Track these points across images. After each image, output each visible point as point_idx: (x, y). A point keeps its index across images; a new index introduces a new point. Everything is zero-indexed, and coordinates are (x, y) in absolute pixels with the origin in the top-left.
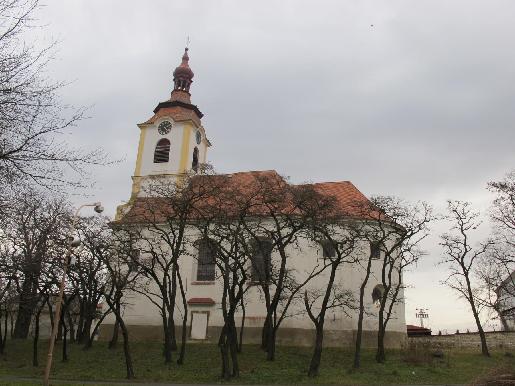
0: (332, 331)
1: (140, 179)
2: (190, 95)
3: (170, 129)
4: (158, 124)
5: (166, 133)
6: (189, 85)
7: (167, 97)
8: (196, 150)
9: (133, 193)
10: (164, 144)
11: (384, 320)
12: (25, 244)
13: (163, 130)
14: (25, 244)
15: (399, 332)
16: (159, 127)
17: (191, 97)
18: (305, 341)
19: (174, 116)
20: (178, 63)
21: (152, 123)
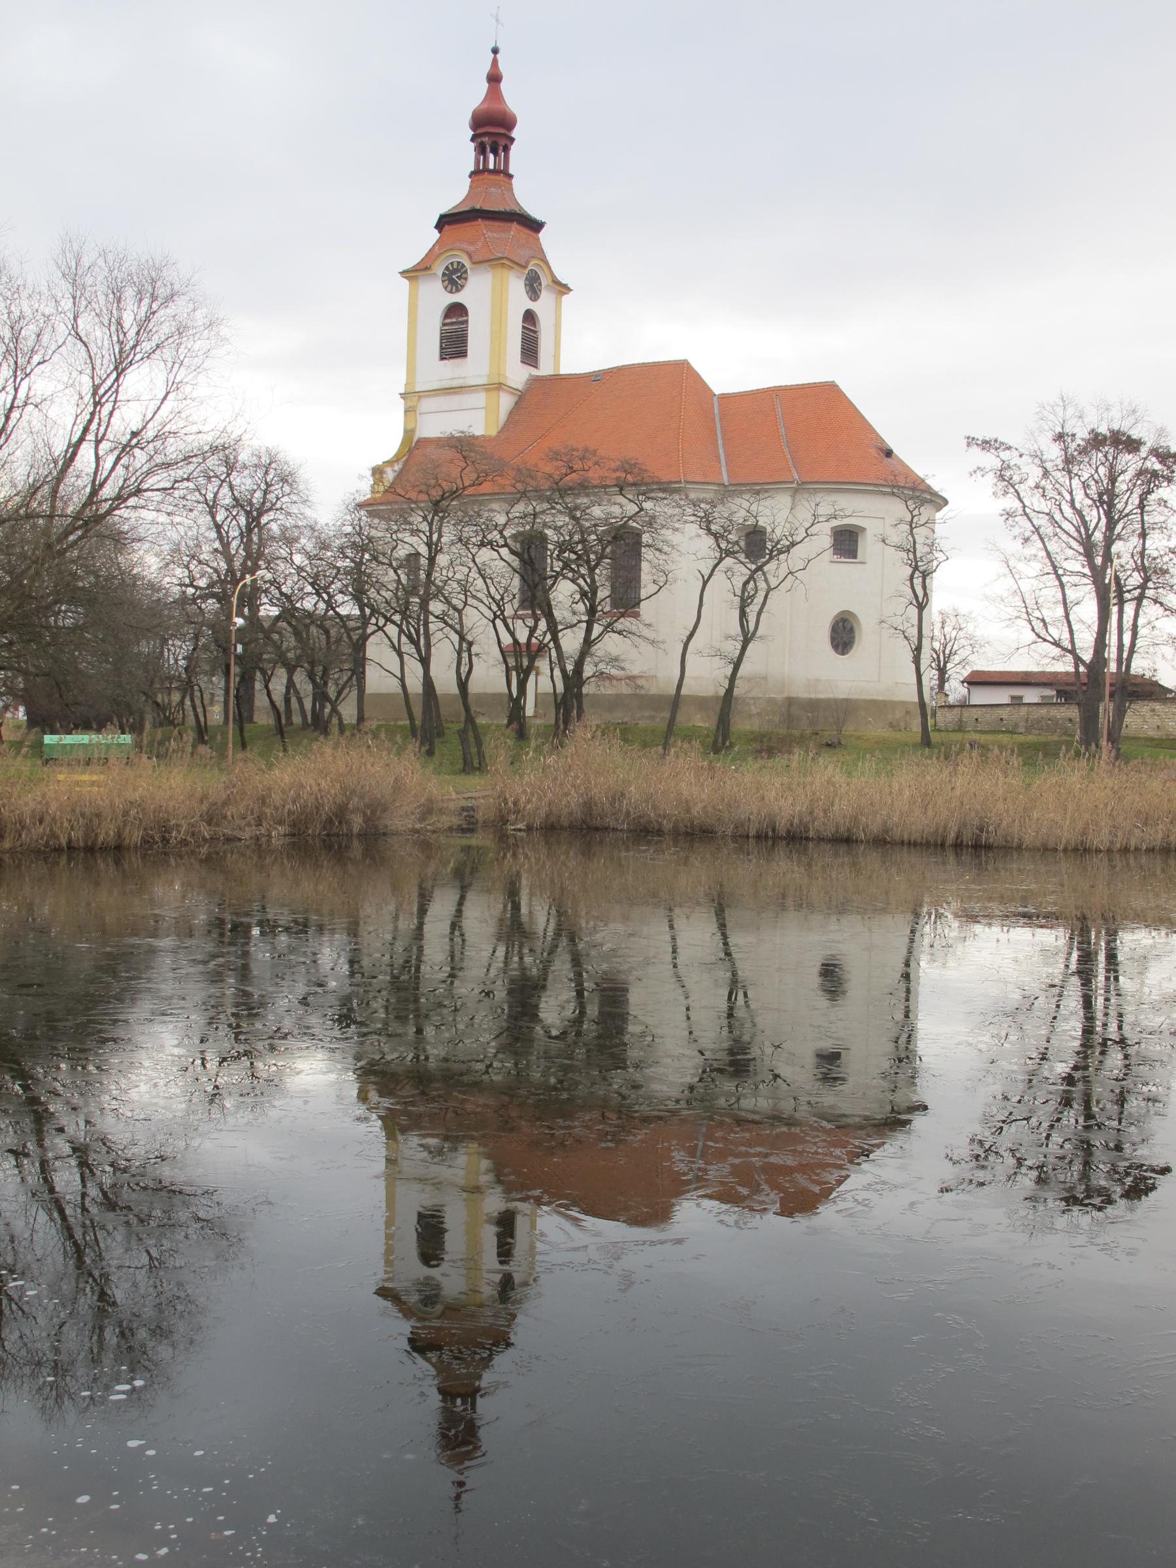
1: (415, 399)
2: (511, 177)
3: (466, 279)
4: (439, 269)
5: (458, 290)
6: (506, 149)
7: (454, 192)
9: (406, 431)
10: (456, 311)
11: (1125, 655)
12: (220, 549)
13: (453, 282)
14: (220, 549)
15: (883, 701)
16: (444, 275)
17: (514, 181)
19: (471, 248)
20: (476, 95)
21: (426, 269)
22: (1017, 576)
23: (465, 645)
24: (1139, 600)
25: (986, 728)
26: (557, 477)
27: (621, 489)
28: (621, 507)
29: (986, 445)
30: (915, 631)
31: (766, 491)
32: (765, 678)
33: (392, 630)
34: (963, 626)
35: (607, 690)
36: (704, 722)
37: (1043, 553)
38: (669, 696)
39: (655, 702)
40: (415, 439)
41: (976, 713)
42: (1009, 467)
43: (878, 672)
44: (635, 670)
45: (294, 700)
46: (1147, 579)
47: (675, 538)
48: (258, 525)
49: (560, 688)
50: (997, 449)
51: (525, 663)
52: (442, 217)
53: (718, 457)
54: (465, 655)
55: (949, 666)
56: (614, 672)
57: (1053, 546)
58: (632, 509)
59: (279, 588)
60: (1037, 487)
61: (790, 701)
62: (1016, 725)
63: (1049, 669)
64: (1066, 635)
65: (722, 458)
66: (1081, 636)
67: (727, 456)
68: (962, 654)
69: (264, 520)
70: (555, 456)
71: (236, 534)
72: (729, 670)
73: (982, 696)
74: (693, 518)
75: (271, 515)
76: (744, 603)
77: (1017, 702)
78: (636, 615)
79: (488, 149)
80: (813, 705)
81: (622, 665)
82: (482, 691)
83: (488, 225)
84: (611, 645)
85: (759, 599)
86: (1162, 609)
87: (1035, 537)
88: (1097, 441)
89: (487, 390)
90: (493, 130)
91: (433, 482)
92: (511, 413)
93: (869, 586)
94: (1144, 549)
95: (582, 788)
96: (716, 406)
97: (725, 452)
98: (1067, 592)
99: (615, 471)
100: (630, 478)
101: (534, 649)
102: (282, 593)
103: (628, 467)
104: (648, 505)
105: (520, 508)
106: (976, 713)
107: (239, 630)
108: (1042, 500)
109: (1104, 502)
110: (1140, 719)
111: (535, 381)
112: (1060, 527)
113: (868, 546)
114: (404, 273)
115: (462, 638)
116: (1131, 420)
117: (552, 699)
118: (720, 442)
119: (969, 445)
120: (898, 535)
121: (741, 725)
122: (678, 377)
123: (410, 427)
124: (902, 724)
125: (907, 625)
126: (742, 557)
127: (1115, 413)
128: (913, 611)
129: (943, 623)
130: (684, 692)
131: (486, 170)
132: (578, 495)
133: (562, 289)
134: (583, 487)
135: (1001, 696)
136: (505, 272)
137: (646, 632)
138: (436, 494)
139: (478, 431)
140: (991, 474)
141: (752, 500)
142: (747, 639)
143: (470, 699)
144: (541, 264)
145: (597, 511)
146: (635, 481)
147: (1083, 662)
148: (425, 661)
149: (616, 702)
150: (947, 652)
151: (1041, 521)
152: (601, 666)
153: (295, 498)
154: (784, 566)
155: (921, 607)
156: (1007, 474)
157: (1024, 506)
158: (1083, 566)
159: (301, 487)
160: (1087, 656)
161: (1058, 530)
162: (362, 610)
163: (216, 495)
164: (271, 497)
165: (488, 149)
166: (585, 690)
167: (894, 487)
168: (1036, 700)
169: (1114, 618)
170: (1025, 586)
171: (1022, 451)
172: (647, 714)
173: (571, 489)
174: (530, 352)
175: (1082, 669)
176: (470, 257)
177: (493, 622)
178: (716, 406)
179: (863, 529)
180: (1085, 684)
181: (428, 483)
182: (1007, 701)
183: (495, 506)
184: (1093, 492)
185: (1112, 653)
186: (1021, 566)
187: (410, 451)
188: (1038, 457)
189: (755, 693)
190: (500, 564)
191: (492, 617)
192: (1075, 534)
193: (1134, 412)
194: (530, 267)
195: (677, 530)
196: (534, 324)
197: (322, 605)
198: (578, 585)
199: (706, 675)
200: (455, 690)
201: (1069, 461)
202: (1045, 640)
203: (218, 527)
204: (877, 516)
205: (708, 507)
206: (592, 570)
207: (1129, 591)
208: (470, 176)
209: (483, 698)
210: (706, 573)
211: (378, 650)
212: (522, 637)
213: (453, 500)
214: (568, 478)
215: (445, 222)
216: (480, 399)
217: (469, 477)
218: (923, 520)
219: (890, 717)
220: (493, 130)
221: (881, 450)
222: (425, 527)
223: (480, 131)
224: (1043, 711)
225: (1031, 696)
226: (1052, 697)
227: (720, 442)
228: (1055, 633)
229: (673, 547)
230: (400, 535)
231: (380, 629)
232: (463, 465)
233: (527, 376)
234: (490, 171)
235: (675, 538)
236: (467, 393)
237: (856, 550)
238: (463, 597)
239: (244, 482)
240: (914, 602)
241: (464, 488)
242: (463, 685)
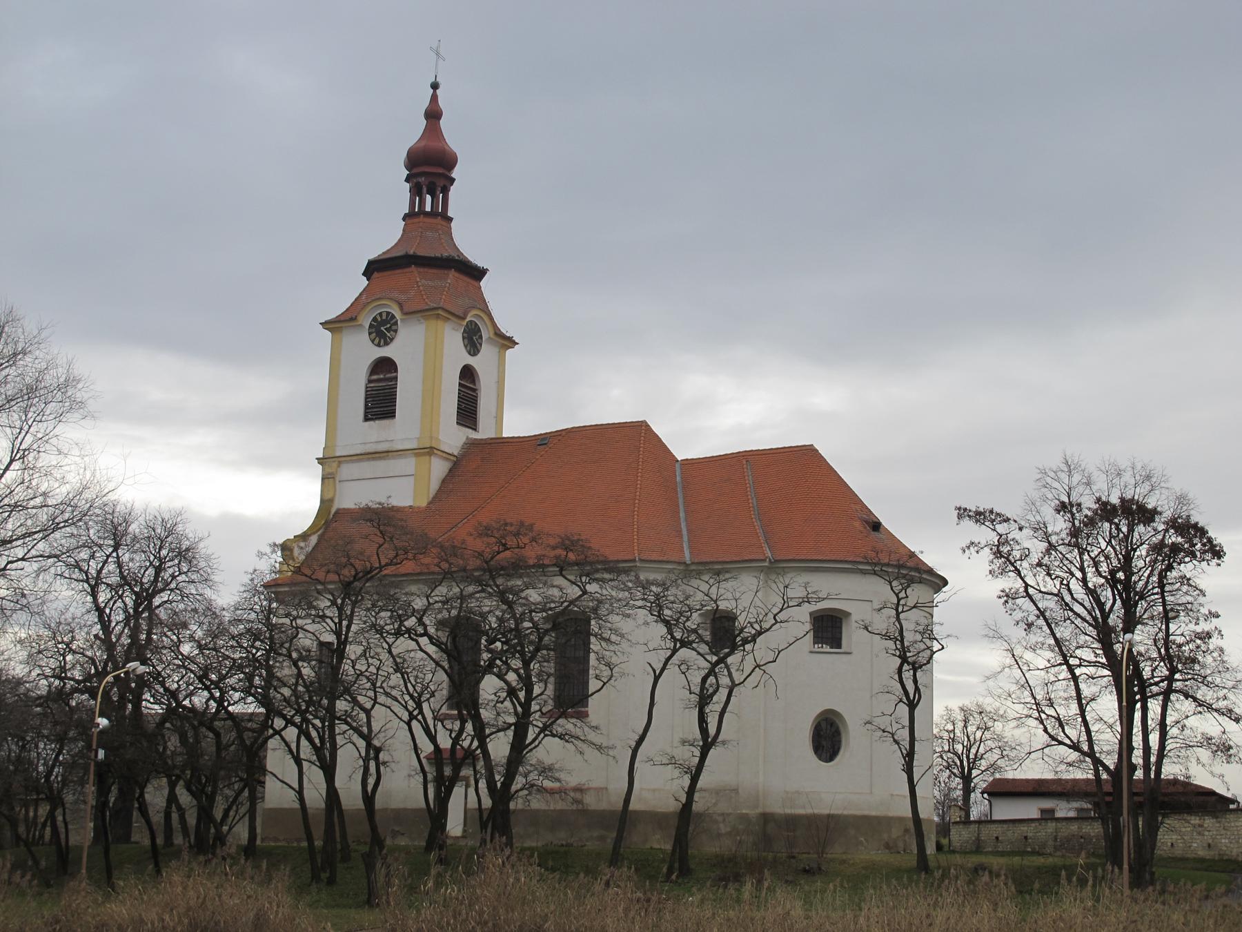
0: (720, 815)
1: (335, 465)
3: (396, 331)
4: (366, 320)
5: (386, 344)
6: (445, 191)
7: (386, 236)
8: (468, 374)
9: (322, 501)
10: (384, 368)
11: (1153, 759)
15: (877, 818)
16: (371, 326)
18: (658, 836)
19: (403, 297)
20: (413, 131)
22: (1025, 668)
23: (373, 752)
24: (1167, 694)
25: (1008, 848)
26: (487, 556)
27: (561, 570)
28: (561, 589)
29: (980, 517)
30: (906, 732)
31: (727, 571)
32: (736, 790)
33: (291, 733)
34: (990, 724)
35: (537, 803)
36: (662, 843)
37: (1052, 642)
38: (612, 813)
39: (599, 819)
40: (333, 511)
41: (995, 830)
42: (1007, 541)
43: (862, 784)
44: (572, 780)
45: (175, 816)
46: (1173, 670)
47: (625, 625)
48: (149, 608)
49: (487, 802)
50: (992, 521)
51: (448, 771)
52: (370, 263)
53: (680, 531)
54: (372, 764)
55: (975, 773)
56: (547, 784)
57: (1064, 631)
58: (574, 592)
59: (163, 684)
60: (1039, 564)
61: (766, 818)
62: (1044, 845)
63: (1065, 776)
64: (1084, 737)
65: (685, 532)
66: (1102, 737)
67: (689, 531)
68: (993, 757)
69: (157, 601)
70: (486, 531)
71: (121, 617)
72: (686, 781)
73: (1007, 810)
74: (640, 603)
75: (165, 596)
76: (704, 700)
77: (1048, 815)
78: (582, 716)
79: (425, 190)
80: (792, 822)
81: (557, 775)
82: (402, 806)
83: (425, 274)
84: (548, 750)
85: (722, 695)
86: (1193, 704)
87: (1041, 622)
88: (1106, 511)
89: (417, 455)
90: (430, 169)
91: (344, 560)
92: (443, 481)
93: (853, 681)
94: (1168, 634)
95: (490, 924)
96: (678, 473)
97: (688, 526)
98: (1082, 686)
99: (554, 548)
100: (572, 556)
101: (460, 754)
102: (166, 690)
103: (568, 544)
104: (592, 588)
105: (442, 590)
106: (995, 830)
107: (102, 732)
108: (1048, 579)
109: (1120, 581)
110: (1178, 836)
111: (471, 445)
112: (1071, 610)
113: (852, 635)
114: (326, 325)
115: (369, 745)
116: (1147, 486)
117: (477, 814)
118: (682, 515)
119: (960, 517)
120: (883, 621)
121: (705, 847)
122: (636, 438)
123: (328, 496)
124: (901, 845)
125: (896, 727)
126: (704, 648)
127: (1128, 478)
128: (904, 710)
129: (966, 721)
130: (632, 806)
131: (422, 212)
132: (509, 576)
133: (508, 342)
134: (517, 568)
135: (1029, 809)
136: (440, 323)
137: (592, 736)
138: (348, 573)
139: (398, 501)
140: (987, 550)
141: (711, 581)
142: (707, 746)
143: (377, 818)
144: (486, 318)
145: (534, 596)
146: (580, 561)
147: (1106, 768)
148: (329, 770)
149: (556, 820)
150: (972, 756)
151: (1049, 604)
152: (533, 776)
153: (194, 577)
154: (749, 658)
155: (912, 706)
156: (1005, 549)
157: (1027, 586)
158: (1097, 655)
159: (202, 564)
160: (1111, 761)
161: (1071, 614)
162: (228, 712)
163: (99, 572)
164: (166, 575)
165: (425, 190)
166: (512, 806)
167: (876, 565)
168: (1072, 814)
169: (1138, 715)
170: (1035, 678)
171: (1023, 523)
172: (596, 834)
173: (502, 568)
174: (468, 413)
175: (1105, 776)
176: (401, 306)
177: (409, 724)
178: (678, 473)
179: (848, 614)
180: (1109, 794)
181: (340, 560)
182: (1035, 814)
183: (413, 588)
184: (1104, 568)
185: (1137, 757)
186: (1028, 656)
187: (327, 524)
188: (1041, 530)
189: (723, 807)
190: (421, 654)
191: (406, 717)
192: (1088, 618)
193: (1148, 477)
194: (468, 319)
195: (628, 616)
196: (473, 382)
197: (213, 704)
198: (506, 682)
199: (659, 788)
200: (360, 804)
201: (1075, 533)
202: (1061, 743)
203: (100, 611)
204: (860, 597)
205: (660, 590)
206: (526, 664)
207: (1156, 684)
208: (404, 219)
209: (400, 816)
210: (658, 668)
211: (276, 759)
212: (445, 742)
213: (368, 580)
214: (502, 555)
215: (374, 268)
216: (408, 465)
217: (387, 554)
218: (911, 603)
219: (885, 836)
220: (430, 169)
221: (867, 522)
222: (333, 612)
223: (415, 171)
224: (1074, 827)
225: (1064, 809)
226: (1088, 810)
227: (682, 515)
228: (1073, 733)
229: (622, 636)
230: (299, 622)
231: (278, 732)
232: (381, 541)
233: (464, 439)
234: (427, 214)
235: (625, 625)
236: (394, 458)
237: (840, 639)
238: (371, 694)
239: (135, 561)
240: (905, 699)
241: (381, 568)
242: (369, 799)
